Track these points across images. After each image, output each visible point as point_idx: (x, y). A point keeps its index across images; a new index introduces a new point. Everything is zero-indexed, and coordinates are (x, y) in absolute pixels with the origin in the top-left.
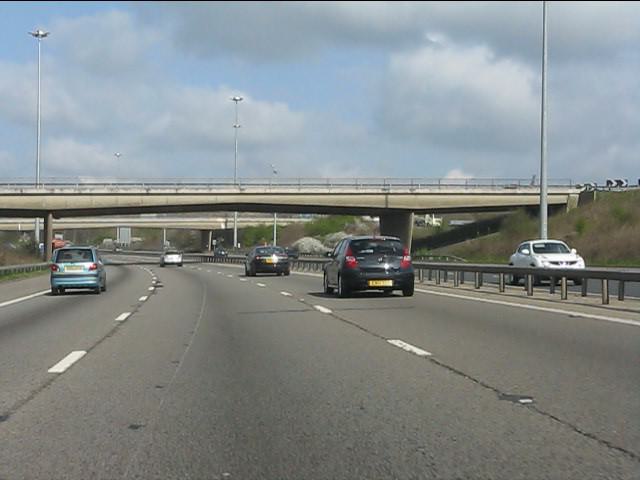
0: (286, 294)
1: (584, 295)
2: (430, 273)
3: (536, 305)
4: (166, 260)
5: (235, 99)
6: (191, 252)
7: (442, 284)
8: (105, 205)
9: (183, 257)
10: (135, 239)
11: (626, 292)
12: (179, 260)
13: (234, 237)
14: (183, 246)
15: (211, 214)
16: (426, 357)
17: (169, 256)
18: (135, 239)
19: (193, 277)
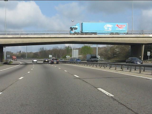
0: (77, 77)
1: (135, 70)
2: (122, 66)
3: (97, 69)
4: (34, 61)
5: (72, 21)
6: (114, 62)
7: (106, 68)
8: (20, 42)
9: (37, 60)
10: (80, 56)
11: (145, 69)
12: (36, 61)
13: (53, 54)
14: (109, 58)
15: (3, 56)
16: (112, 97)
17: (34, 60)
18: (80, 56)
19: (46, 68)
